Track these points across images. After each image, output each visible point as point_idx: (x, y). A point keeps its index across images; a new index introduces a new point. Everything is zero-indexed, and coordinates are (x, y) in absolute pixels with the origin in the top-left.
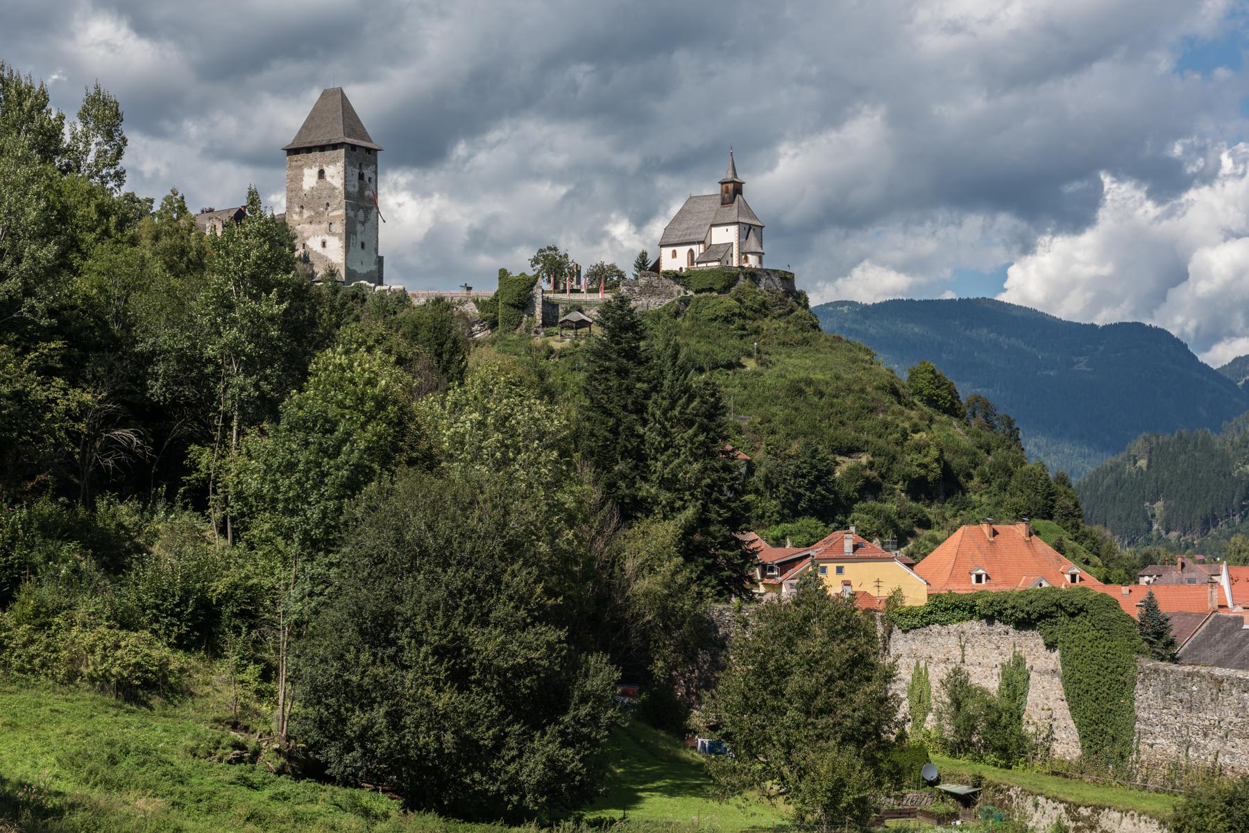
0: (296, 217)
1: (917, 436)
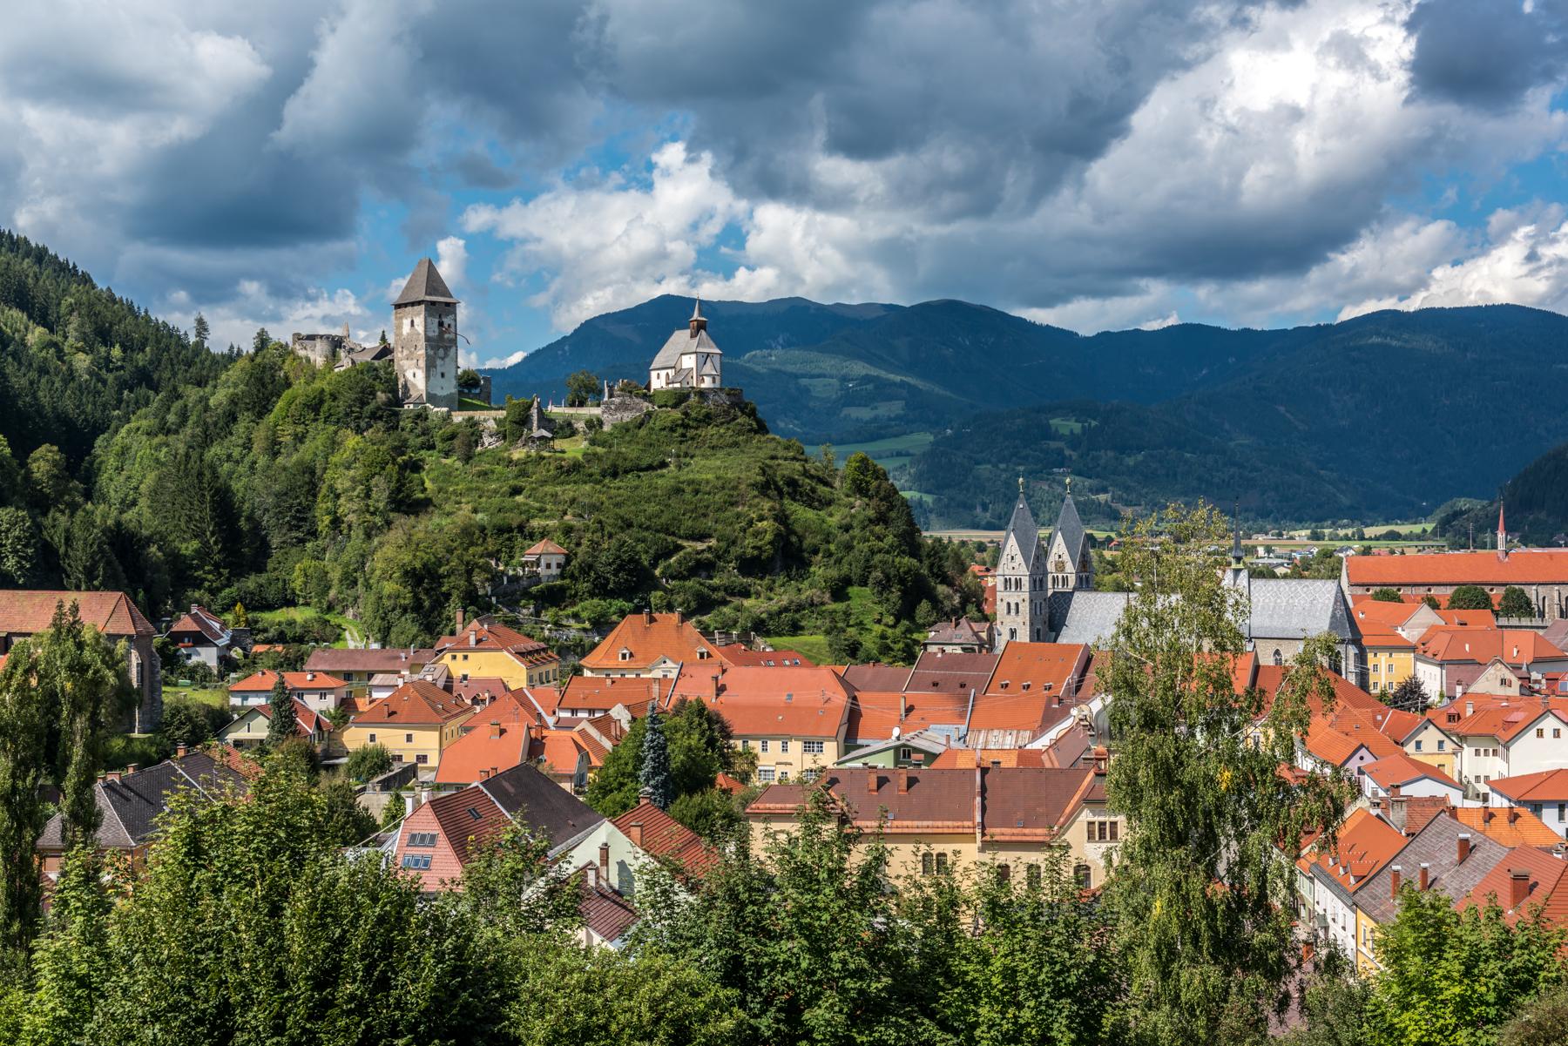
1: (760, 524)
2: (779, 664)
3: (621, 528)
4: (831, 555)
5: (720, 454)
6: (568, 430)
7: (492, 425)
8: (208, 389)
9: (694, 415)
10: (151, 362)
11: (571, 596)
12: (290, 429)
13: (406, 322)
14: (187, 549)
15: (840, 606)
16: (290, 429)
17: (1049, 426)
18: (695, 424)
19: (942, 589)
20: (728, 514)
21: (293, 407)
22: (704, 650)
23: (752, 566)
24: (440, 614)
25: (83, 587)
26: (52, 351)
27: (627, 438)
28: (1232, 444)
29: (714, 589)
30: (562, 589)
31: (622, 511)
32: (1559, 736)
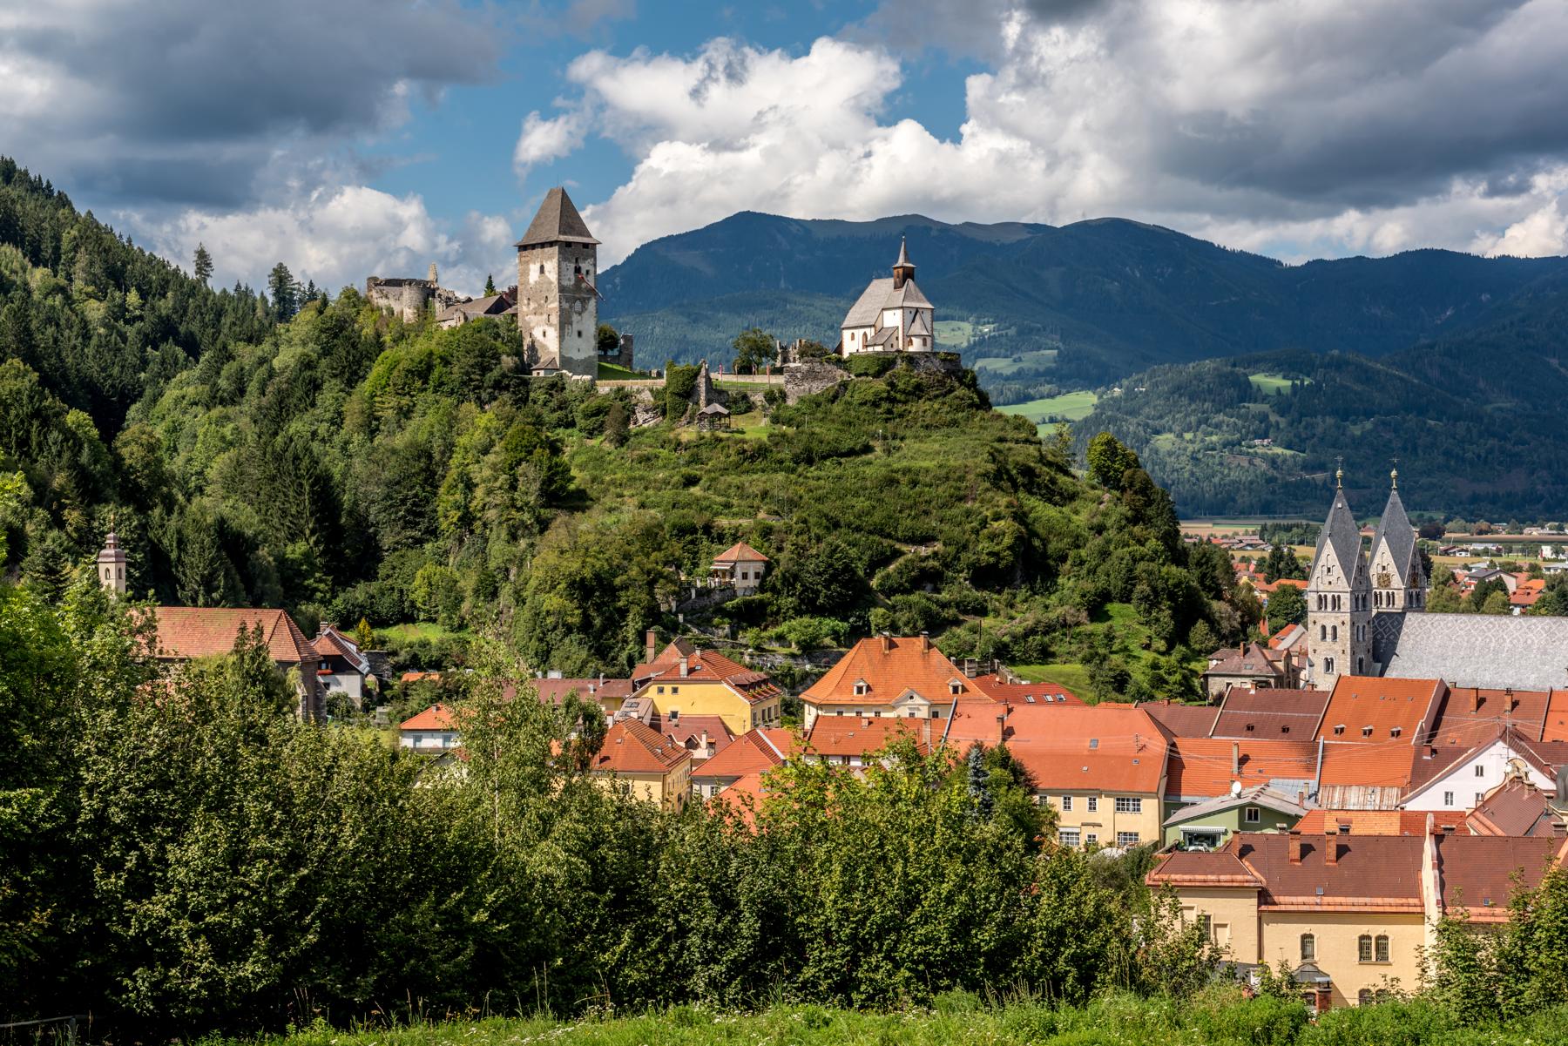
0: (525, 308)
1: (995, 524)
2: (1040, 702)
3: (827, 528)
4: (1082, 563)
5: (936, 435)
6: (741, 403)
7: (647, 397)
8: (266, 346)
9: (901, 386)
10: (175, 311)
11: (772, 614)
12: (393, 401)
13: (534, 269)
14: (293, 552)
15: (1100, 628)
16: (393, 401)
17: (1249, 384)
18: (903, 398)
19: (1216, 605)
20: (955, 511)
21: (395, 373)
22: (958, 683)
23: (987, 576)
24: (614, 635)
25: (201, 600)
26: (59, 297)
27: (819, 415)
28: (1489, 408)
29: (944, 605)
30: (762, 605)
31: (825, 508)
32: (1447, 794)
